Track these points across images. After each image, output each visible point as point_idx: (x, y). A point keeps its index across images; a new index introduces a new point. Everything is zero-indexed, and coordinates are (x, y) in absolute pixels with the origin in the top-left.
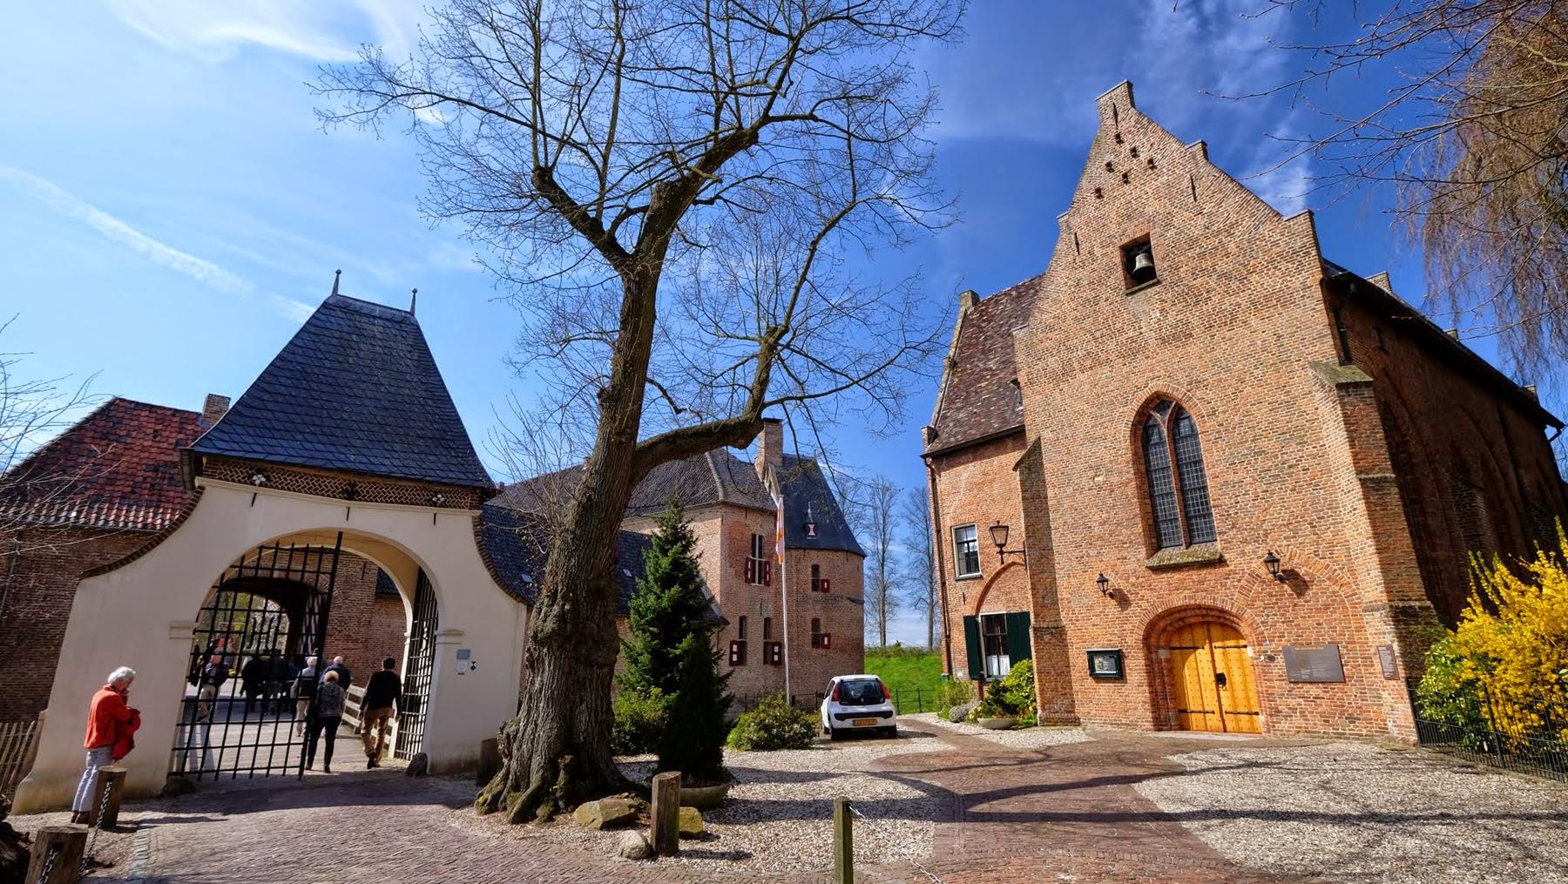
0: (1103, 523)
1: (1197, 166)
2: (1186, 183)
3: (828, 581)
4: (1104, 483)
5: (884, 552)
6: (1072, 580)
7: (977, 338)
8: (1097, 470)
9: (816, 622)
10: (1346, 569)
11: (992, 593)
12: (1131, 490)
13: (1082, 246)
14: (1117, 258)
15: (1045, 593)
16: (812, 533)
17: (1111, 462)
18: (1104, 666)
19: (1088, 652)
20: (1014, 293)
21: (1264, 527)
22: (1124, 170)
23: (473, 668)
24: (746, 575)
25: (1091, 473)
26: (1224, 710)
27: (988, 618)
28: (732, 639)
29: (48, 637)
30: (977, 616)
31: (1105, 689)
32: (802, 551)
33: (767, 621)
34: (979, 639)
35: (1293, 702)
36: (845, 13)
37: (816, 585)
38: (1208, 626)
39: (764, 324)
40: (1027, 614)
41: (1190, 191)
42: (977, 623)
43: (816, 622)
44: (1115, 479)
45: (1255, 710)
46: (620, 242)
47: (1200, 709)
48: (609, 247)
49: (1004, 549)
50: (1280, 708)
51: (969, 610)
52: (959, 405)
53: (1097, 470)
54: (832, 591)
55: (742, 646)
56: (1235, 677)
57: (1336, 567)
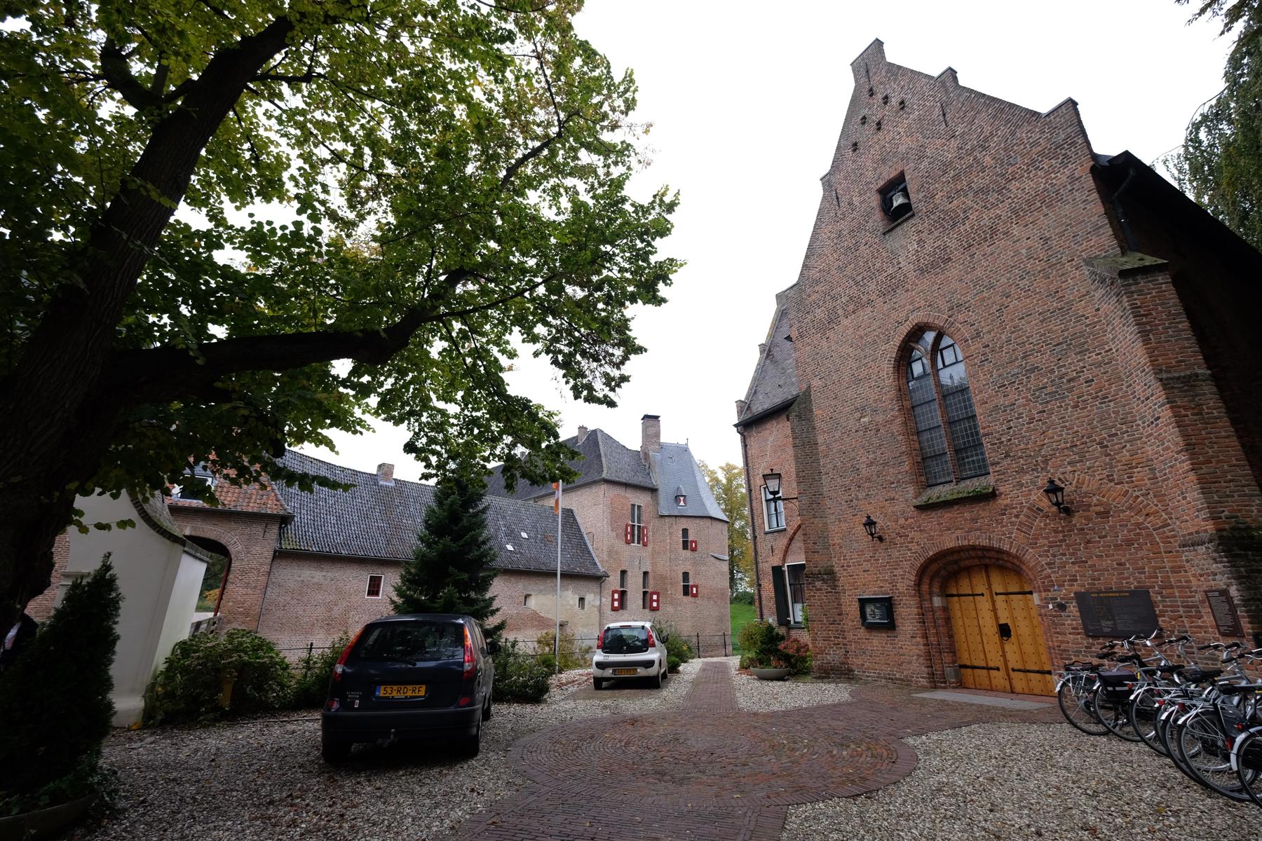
4: (870, 422)
9: (686, 576)
12: (896, 427)
17: (875, 401)
21: (1043, 452)
25: (857, 415)
33: (646, 574)
34: (785, 586)
37: (685, 545)
43: (686, 576)
45: (1047, 668)
51: (776, 561)
56: (1022, 628)
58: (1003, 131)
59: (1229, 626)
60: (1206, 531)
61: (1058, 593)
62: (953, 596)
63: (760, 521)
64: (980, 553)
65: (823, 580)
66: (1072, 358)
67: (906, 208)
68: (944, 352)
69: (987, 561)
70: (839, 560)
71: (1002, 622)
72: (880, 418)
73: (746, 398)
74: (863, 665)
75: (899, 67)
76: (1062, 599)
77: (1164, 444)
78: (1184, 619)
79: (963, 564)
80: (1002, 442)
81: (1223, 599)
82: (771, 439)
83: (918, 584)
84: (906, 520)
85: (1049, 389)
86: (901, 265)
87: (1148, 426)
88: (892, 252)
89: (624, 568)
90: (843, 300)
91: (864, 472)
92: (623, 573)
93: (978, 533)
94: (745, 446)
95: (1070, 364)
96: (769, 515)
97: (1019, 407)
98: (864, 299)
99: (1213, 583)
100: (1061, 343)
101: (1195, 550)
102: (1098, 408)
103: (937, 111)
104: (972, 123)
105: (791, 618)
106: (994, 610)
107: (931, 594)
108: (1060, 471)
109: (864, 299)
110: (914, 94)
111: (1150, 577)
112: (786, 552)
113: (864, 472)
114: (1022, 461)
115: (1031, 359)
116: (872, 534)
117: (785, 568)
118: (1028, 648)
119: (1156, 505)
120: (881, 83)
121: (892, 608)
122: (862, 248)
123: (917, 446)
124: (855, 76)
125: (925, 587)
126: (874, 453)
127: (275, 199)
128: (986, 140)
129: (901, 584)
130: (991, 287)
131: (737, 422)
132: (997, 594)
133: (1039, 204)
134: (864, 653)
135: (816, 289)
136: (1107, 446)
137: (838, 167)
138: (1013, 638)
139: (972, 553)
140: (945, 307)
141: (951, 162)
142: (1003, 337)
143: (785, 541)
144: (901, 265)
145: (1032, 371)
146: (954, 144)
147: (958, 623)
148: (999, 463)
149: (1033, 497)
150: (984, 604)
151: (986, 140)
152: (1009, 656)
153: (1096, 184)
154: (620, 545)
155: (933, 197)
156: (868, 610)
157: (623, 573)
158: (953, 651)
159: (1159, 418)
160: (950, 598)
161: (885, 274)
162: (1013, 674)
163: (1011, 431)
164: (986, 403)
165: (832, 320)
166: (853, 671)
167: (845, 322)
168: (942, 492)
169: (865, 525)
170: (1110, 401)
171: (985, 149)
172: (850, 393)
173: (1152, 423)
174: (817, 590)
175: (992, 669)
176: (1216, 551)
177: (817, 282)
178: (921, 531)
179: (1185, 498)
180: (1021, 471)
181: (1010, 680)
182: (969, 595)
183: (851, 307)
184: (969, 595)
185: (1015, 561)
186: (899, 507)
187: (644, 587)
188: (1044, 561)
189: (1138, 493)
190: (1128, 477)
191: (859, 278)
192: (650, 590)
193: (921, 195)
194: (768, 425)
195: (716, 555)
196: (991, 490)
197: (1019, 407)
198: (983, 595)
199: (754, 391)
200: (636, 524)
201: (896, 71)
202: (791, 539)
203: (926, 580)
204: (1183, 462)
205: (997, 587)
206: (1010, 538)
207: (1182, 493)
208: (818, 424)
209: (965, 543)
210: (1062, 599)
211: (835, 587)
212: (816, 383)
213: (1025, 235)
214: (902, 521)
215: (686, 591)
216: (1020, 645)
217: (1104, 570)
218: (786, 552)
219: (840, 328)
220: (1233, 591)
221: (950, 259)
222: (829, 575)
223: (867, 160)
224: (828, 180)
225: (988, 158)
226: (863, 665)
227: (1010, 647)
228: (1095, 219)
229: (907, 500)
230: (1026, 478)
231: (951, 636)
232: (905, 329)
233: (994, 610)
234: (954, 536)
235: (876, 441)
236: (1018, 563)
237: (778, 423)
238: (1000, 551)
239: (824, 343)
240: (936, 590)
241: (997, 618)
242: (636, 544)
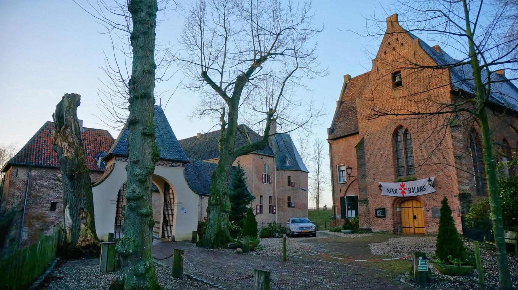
0: (382, 167)
1: (416, 47)
2: (413, 53)
3: (294, 183)
4: (383, 154)
5: (319, 169)
6: (372, 185)
7: (349, 94)
8: (381, 149)
9: (289, 198)
10: (450, 184)
11: (350, 188)
12: (391, 157)
13: (379, 72)
14: (390, 77)
15: (363, 189)
16: (288, 164)
17: (385, 147)
18: (379, 213)
19: (375, 209)
20: (363, 76)
21: (429, 170)
22: (394, 46)
23: (185, 213)
24: (262, 180)
25: (379, 151)
26: (415, 226)
27: (348, 197)
28: (257, 204)
29: (40, 201)
30: (345, 196)
31: (380, 220)
32: (284, 171)
33: (270, 197)
34: (345, 204)
35: (433, 224)
36: (292, 27)
37: (289, 184)
38: (412, 201)
39: (268, 108)
40: (358, 196)
41: (414, 56)
42: (345, 199)
43: (289, 198)
44: (386, 153)
45: (424, 227)
46: (227, 94)
47: (409, 226)
48: (224, 95)
49: (350, 175)
50: (430, 226)
51: (342, 195)
52: (341, 120)
53: (381, 149)
54: (295, 186)
55: (261, 206)
56: (419, 217)
57: (448, 183)
63: (336, 179)
71: (415, 215)
83: (393, 205)
89: (261, 195)
91: (380, 169)
92: (261, 196)
94: (331, 148)
96: (340, 177)
105: (347, 216)
106: (413, 212)
107: (396, 207)
112: (346, 192)
113: (380, 169)
114: (424, 172)
117: (346, 198)
118: (420, 222)
123: (397, 163)
125: (395, 205)
129: (388, 205)
143: (346, 187)
150: (410, 210)
152: (415, 224)
153: (451, 96)
154: (260, 184)
157: (261, 196)
158: (401, 223)
187: (270, 204)
192: (272, 205)
195: (303, 188)
199: (334, 124)
200: (267, 174)
202: (349, 186)
203: (396, 203)
205: (415, 205)
208: (366, 152)
211: (368, 205)
215: (289, 205)
218: (346, 192)
220: (460, 207)
222: (365, 201)
231: (401, 219)
232: (391, 131)
233: (413, 212)
235: (384, 160)
240: (398, 206)
241: (413, 214)
242: (266, 183)
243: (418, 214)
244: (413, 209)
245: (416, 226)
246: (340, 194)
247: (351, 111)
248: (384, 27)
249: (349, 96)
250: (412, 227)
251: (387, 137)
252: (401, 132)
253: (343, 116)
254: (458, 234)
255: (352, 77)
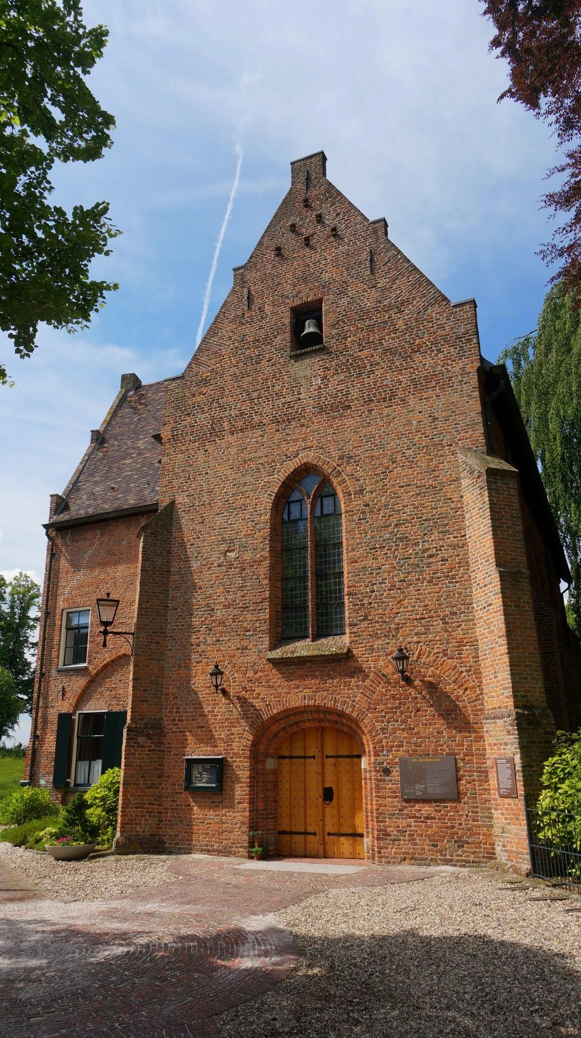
14: (287, 319)
25: (223, 547)
27: (87, 716)
30: (74, 713)
34: (71, 739)
42: (74, 720)
51: (65, 707)
52: (97, 479)
58: (418, 303)
59: (507, 789)
60: (507, 707)
61: (386, 758)
62: (284, 757)
64: (322, 716)
65: (148, 735)
66: (435, 535)
67: (316, 338)
68: (325, 500)
69: (326, 724)
70: (171, 712)
71: (327, 785)
72: (248, 556)
73: (64, 494)
74: (177, 836)
75: (339, 193)
76: (388, 763)
77: (489, 628)
78: (476, 782)
79: (303, 726)
80: (363, 605)
81: (509, 765)
82: (90, 552)
84: (256, 673)
85: (411, 561)
86: (301, 397)
87: (481, 609)
88: (295, 380)
90: (232, 413)
93: (325, 694)
95: (433, 541)
97: (385, 572)
98: (256, 419)
99: (503, 751)
100: (429, 520)
101: (495, 723)
102: (447, 587)
103: (365, 255)
104: (394, 281)
108: (408, 638)
109: (256, 419)
110: (347, 227)
111: (458, 745)
115: (402, 529)
116: (217, 686)
117: (76, 717)
119: (474, 681)
120: (318, 199)
121: (222, 770)
122: (264, 363)
124: (293, 177)
126: (234, 593)
127: (85, 210)
128: (402, 304)
130: (382, 447)
131: (47, 522)
132: (327, 757)
133: (434, 383)
134: (181, 821)
135: (204, 390)
136: (447, 623)
137: (255, 264)
138: (334, 802)
139: (315, 716)
140: (336, 454)
141: (368, 311)
142: (383, 499)
144: (301, 397)
145: (401, 540)
146: (375, 294)
147: (285, 785)
148: (356, 625)
149: (381, 663)
150: (313, 767)
151: (402, 304)
155: (345, 338)
156: (195, 773)
159: (491, 604)
160: (281, 760)
161: (283, 400)
162: (327, 837)
163: (373, 594)
164: (356, 562)
165: (215, 432)
166: (164, 843)
167: (231, 439)
168: (302, 648)
169: (211, 674)
170: (456, 582)
171: (400, 312)
172: (219, 520)
173: (485, 608)
174: (139, 747)
175: (309, 834)
176: (511, 725)
177: (205, 382)
178: (269, 687)
179: (496, 677)
180: (375, 636)
181: (324, 843)
182: (300, 757)
183: (240, 424)
184: (300, 757)
185: (353, 726)
186: (252, 657)
188: (378, 726)
189: (463, 669)
190: (458, 654)
191: (255, 395)
193: (334, 332)
194: (89, 535)
196: (345, 651)
197: (385, 572)
198: (314, 757)
199: (75, 486)
201: (333, 194)
204: (502, 645)
206: (354, 701)
207: (495, 673)
209: (312, 703)
210: (388, 763)
212: (181, 499)
213: (418, 408)
214: (250, 674)
216: (339, 807)
217: (425, 737)
219: (223, 444)
221: (349, 407)
223: (288, 272)
224: (242, 274)
225: (401, 322)
226: (177, 836)
227: (330, 811)
228: (473, 414)
229: (260, 652)
230: (378, 643)
232: (292, 465)
233: (323, 773)
234: (301, 695)
236: (355, 728)
237: (103, 535)
238: (341, 714)
239: (201, 455)
243: (338, 782)
244: (323, 765)
245: (330, 828)
246: (60, 703)
247: (132, 458)
248: (283, 185)
249: (131, 423)
250: (315, 834)
251: (255, 502)
252: (312, 485)
253: (106, 469)
254: (68, 811)
255: (143, 383)
